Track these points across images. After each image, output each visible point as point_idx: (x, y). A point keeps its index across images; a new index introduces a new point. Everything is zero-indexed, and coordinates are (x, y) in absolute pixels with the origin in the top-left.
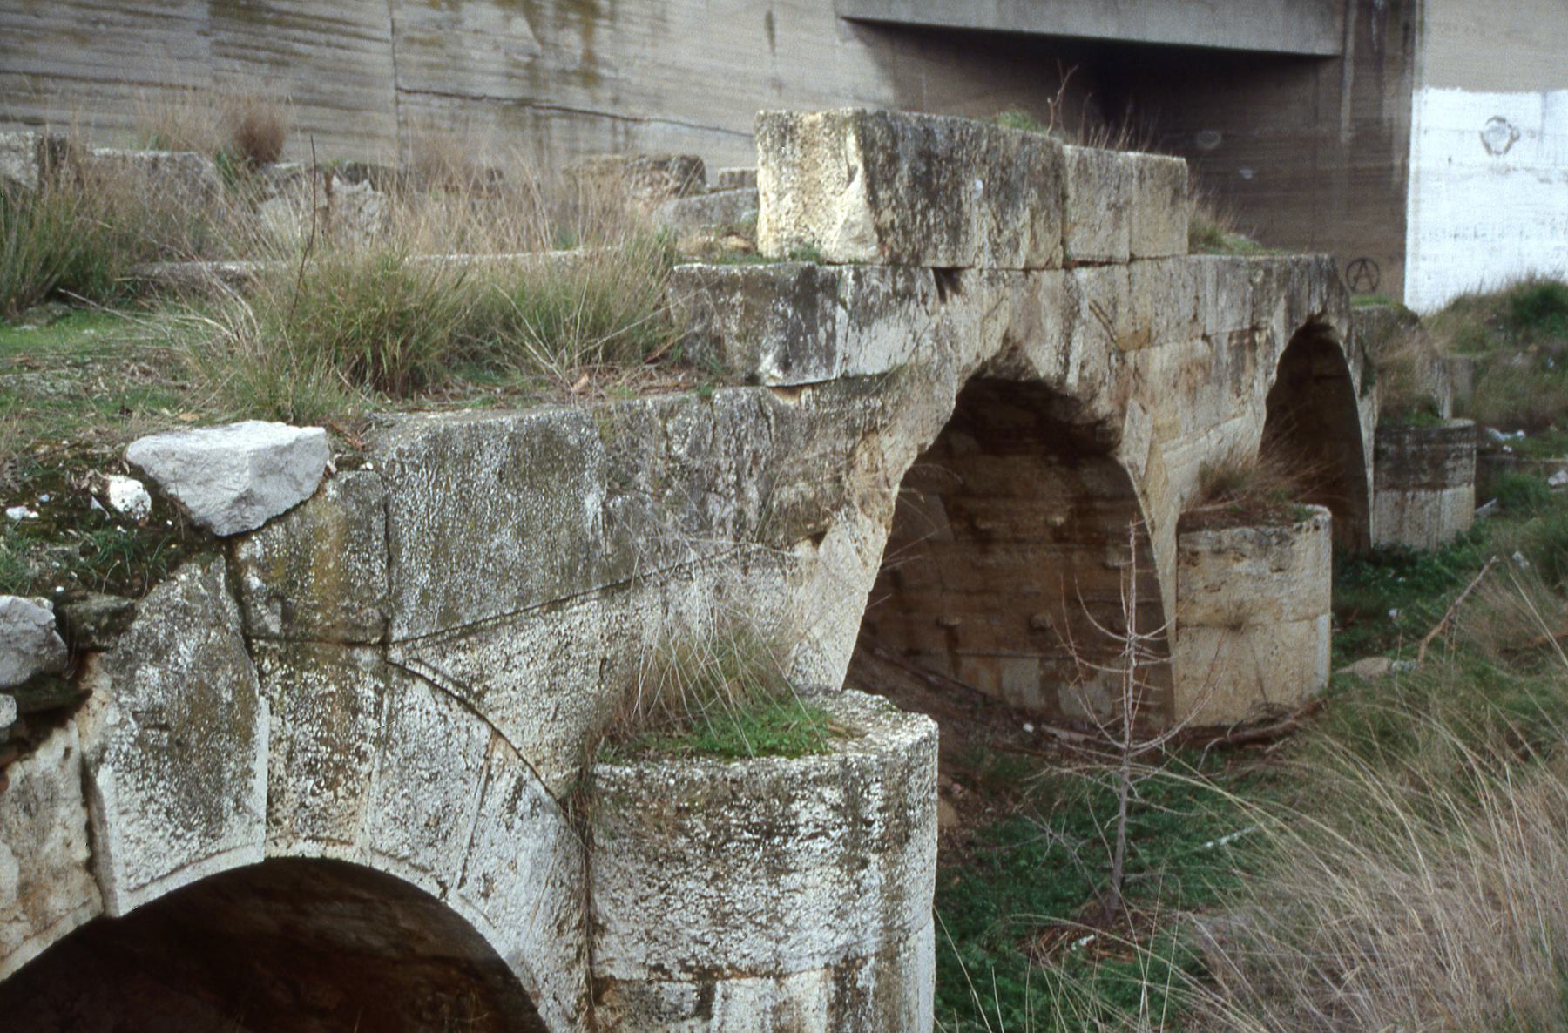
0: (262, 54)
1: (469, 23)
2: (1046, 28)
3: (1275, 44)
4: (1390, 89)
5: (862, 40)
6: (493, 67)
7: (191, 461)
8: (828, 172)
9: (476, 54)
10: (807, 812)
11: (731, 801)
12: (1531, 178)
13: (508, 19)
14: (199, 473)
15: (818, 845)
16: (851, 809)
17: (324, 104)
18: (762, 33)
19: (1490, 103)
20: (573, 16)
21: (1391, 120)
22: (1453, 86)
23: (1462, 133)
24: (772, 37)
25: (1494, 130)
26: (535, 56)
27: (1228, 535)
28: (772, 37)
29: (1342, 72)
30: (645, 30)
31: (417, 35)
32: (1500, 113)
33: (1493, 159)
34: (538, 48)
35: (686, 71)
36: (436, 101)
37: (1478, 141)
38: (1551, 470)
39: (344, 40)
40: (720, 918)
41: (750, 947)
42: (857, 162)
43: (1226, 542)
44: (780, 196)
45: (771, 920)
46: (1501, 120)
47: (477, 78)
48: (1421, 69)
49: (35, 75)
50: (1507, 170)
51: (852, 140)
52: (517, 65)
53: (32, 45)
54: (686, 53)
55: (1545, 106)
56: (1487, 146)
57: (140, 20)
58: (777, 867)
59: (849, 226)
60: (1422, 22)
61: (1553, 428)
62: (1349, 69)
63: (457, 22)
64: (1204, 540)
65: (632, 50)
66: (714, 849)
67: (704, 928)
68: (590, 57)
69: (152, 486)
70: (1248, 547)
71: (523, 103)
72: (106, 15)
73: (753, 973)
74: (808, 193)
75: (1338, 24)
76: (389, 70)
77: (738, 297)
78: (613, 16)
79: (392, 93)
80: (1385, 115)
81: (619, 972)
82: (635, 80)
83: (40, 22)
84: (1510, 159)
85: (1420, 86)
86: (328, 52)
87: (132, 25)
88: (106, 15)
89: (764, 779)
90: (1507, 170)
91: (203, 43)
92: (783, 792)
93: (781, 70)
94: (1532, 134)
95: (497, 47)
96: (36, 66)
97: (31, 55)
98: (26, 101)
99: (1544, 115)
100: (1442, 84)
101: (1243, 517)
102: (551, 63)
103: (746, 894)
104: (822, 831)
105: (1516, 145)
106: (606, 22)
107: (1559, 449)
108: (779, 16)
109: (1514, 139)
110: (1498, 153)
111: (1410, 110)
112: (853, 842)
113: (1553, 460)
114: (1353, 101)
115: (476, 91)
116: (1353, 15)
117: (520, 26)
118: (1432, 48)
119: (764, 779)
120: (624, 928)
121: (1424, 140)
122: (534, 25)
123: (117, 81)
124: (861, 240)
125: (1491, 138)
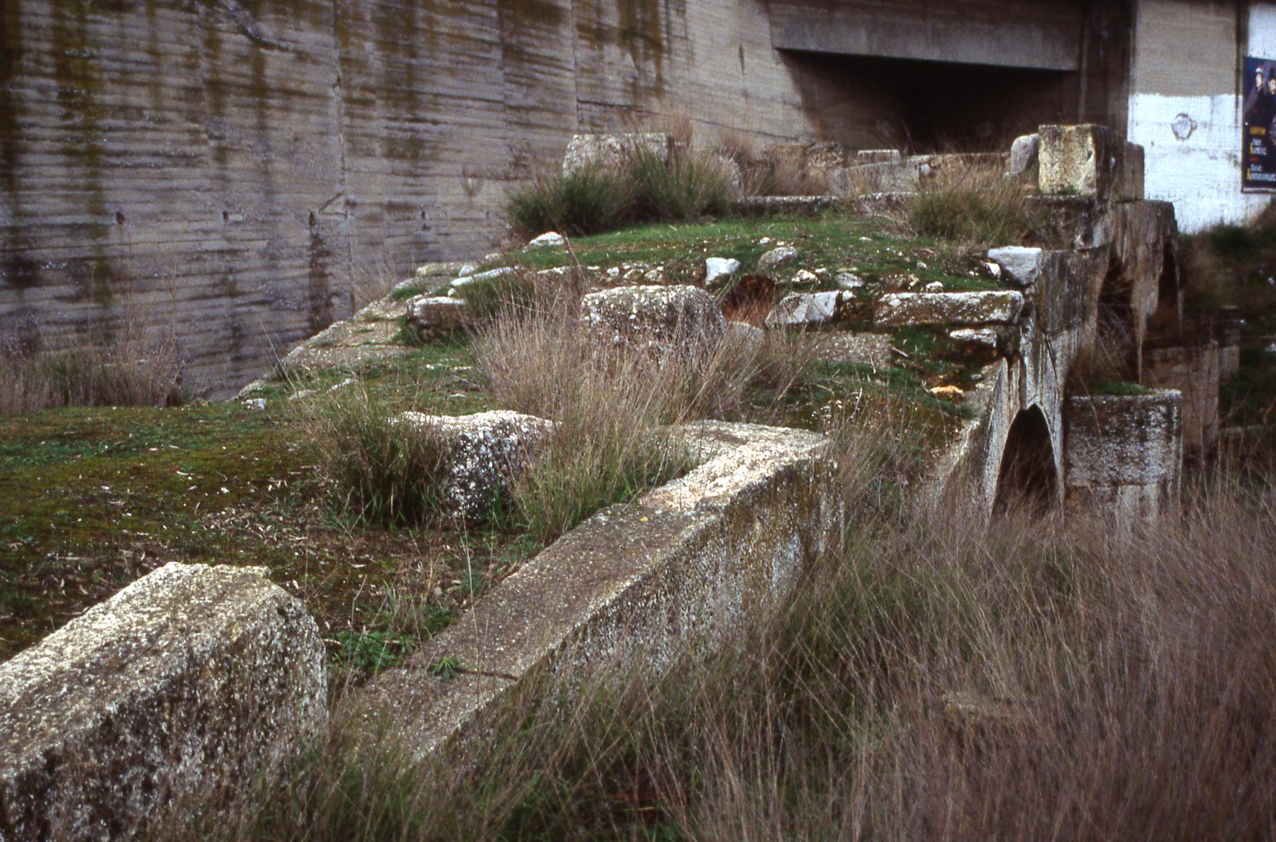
0: (523, 80)
1: (607, 59)
2: (897, 54)
3: (1048, 65)
4: (1113, 95)
5: (787, 64)
6: (617, 85)
7: (1015, 257)
8: (1078, 154)
9: (611, 78)
10: (1154, 416)
11: (1128, 411)
12: (1204, 155)
13: (623, 55)
14: (1017, 262)
15: (1158, 430)
16: (1168, 416)
17: (548, 110)
18: (738, 61)
19: (1179, 103)
20: (651, 52)
21: (1113, 116)
22: (1154, 91)
23: (1160, 125)
24: (742, 62)
25: (1180, 123)
26: (635, 78)
27: (1170, 352)
28: (742, 62)
29: (1079, 83)
30: (683, 60)
31: (586, 67)
32: (1185, 111)
33: (1180, 142)
34: (636, 73)
35: (703, 86)
36: (594, 108)
37: (1170, 131)
38: (1267, 343)
39: (556, 71)
40: (1122, 459)
41: (1131, 472)
42: (1092, 149)
43: (1170, 355)
44: (1053, 165)
45: (1141, 461)
46: (1185, 116)
47: (611, 93)
48: (1134, 81)
49: (436, 95)
50: (1189, 151)
51: (1090, 140)
52: (627, 84)
53: (433, 77)
54: (703, 74)
55: (1213, 105)
56: (1176, 134)
57: (475, 61)
58: (1143, 438)
59: (1087, 178)
60: (1134, 48)
61: (1263, 318)
62: (1084, 80)
63: (602, 57)
64: (1157, 355)
65: (678, 73)
66: (1119, 433)
67: (1114, 464)
68: (660, 79)
69: (1001, 265)
70: (1180, 358)
71: (630, 108)
72: (461, 58)
73: (1132, 483)
74: (1067, 164)
75: (1076, 50)
76: (573, 89)
77: (1063, 210)
78: (669, 52)
79: (575, 103)
80: (1110, 113)
81: (1078, 483)
82: (681, 93)
83: (436, 63)
84: (1190, 143)
85: (1134, 92)
86: (549, 78)
87: (472, 64)
88: (461, 58)
89: (1139, 401)
90: (1189, 151)
91: (500, 74)
92: (1146, 406)
93: (750, 86)
94: (1205, 125)
95: (619, 73)
96: (435, 90)
97: (434, 83)
98: (432, 110)
99: (1212, 111)
100: (1146, 91)
101: (1175, 342)
102: (642, 83)
103: (1132, 449)
104: (1158, 425)
105: (1194, 133)
106: (665, 55)
107: (1271, 330)
108: (745, 48)
109: (1193, 128)
110: (1183, 139)
111: (1127, 109)
112: (1169, 429)
113: (1266, 337)
114: (1087, 102)
115: (611, 101)
116: (1086, 44)
117: (629, 59)
118: (1142, 66)
119: (1139, 401)
120: (1081, 464)
121: (1136, 129)
122: (634, 59)
123: (465, 98)
124: (1091, 186)
125: (1178, 128)
